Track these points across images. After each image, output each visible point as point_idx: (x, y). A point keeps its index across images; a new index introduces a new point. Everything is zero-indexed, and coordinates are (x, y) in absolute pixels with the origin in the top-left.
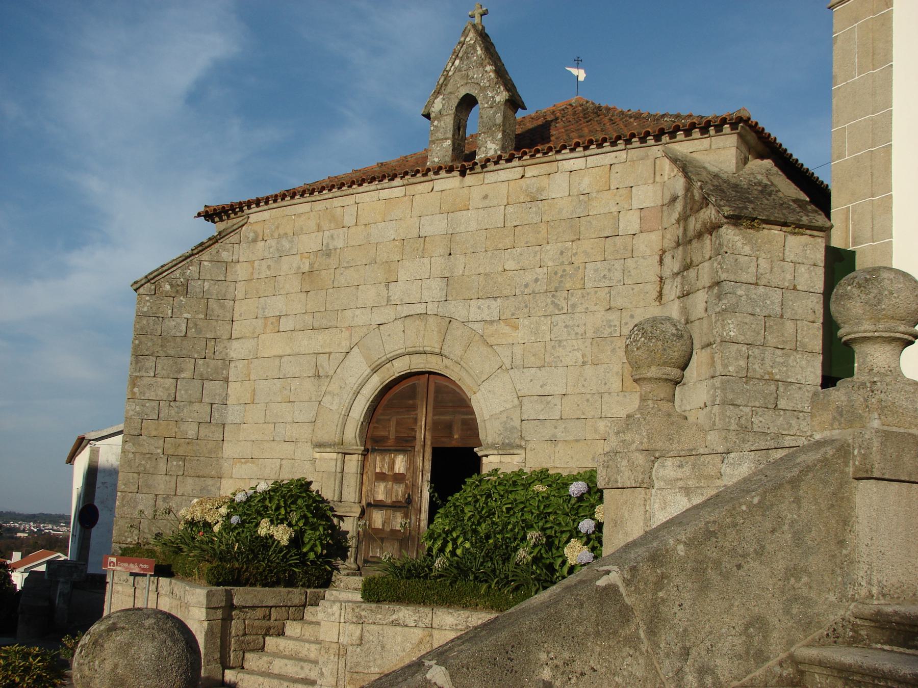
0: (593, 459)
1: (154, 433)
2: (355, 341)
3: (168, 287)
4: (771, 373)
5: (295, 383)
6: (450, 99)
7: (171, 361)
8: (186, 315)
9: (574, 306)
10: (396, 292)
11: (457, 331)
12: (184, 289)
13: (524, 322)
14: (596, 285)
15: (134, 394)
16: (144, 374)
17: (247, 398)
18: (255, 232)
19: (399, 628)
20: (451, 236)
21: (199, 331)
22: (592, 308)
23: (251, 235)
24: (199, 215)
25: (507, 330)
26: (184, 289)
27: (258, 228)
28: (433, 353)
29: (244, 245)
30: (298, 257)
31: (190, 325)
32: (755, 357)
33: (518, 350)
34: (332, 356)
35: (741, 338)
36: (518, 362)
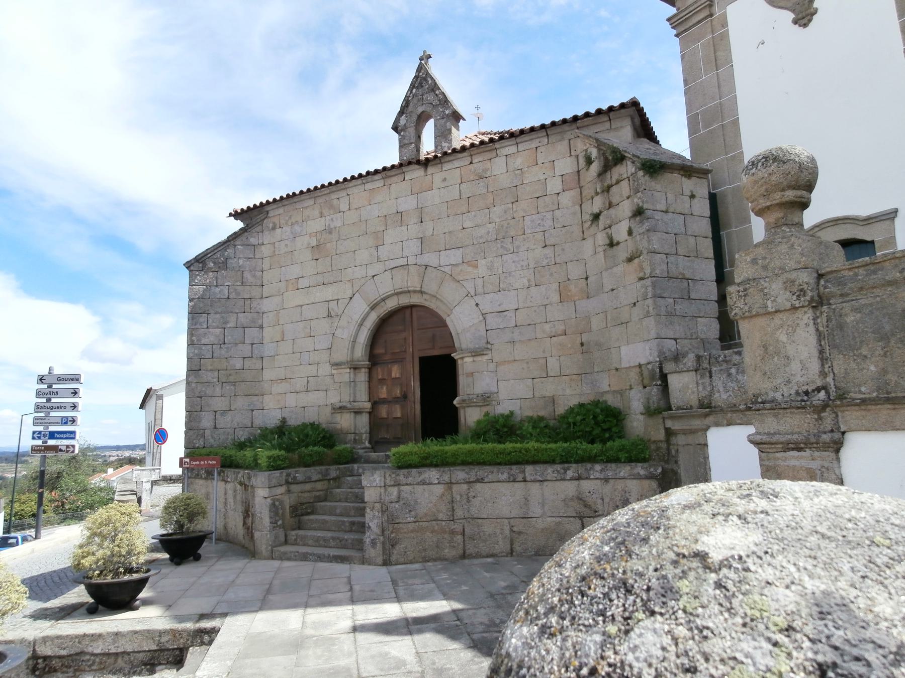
0: (544, 352)
1: (210, 368)
2: (355, 289)
4: (683, 274)
5: (313, 323)
6: (411, 116)
7: (218, 316)
8: (227, 284)
9: (518, 247)
10: (384, 252)
11: (431, 274)
12: (224, 265)
13: (482, 262)
14: (533, 231)
15: (193, 341)
17: (278, 338)
18: (274, 223)
19: (425, 486)
20: (421, 209)
21: (238, 294)
22: (533, 247)
23: (271, 225)
24: (231, 215)
25: (470, 269)
26: (224, 265)
27: (276, 220)
28: (415, 292)
29: (266, 233)
30: (308, 236)
31: (231, 290)
32: (672, 263)
33: (479, 282)
34: (339, 301)
35: (660, 250)
36: (480, 290)
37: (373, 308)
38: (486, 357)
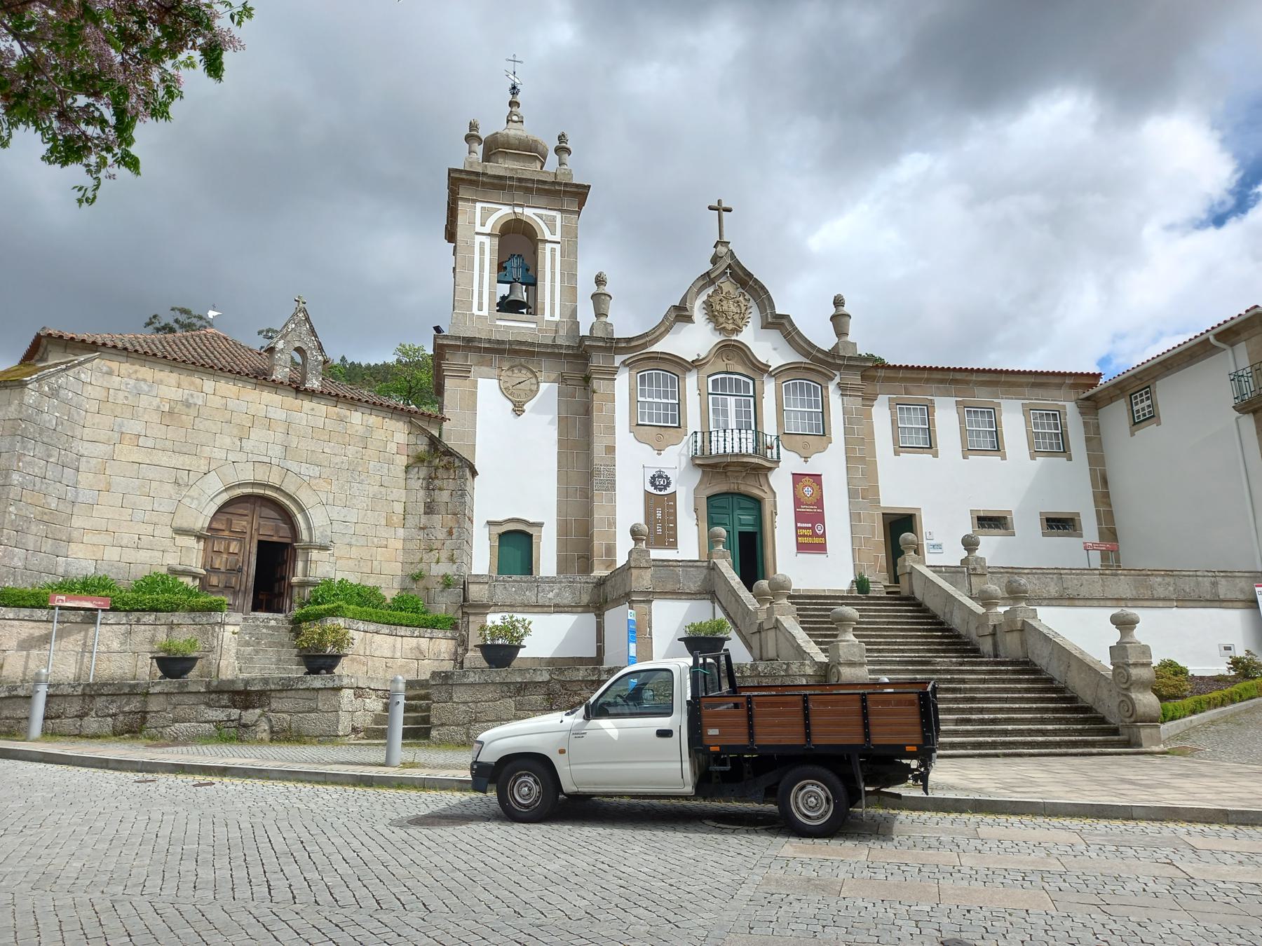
3: (47, 389)
8: (56, 414)
16: (27, 453)
17: (102, 486)
30: (158, 399)
36: (331, 501)
37: (226, 490)
38: (329, 552)
